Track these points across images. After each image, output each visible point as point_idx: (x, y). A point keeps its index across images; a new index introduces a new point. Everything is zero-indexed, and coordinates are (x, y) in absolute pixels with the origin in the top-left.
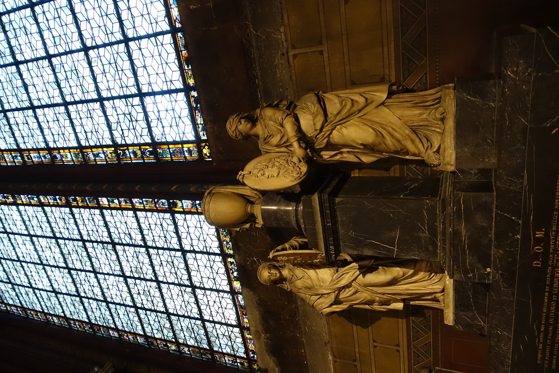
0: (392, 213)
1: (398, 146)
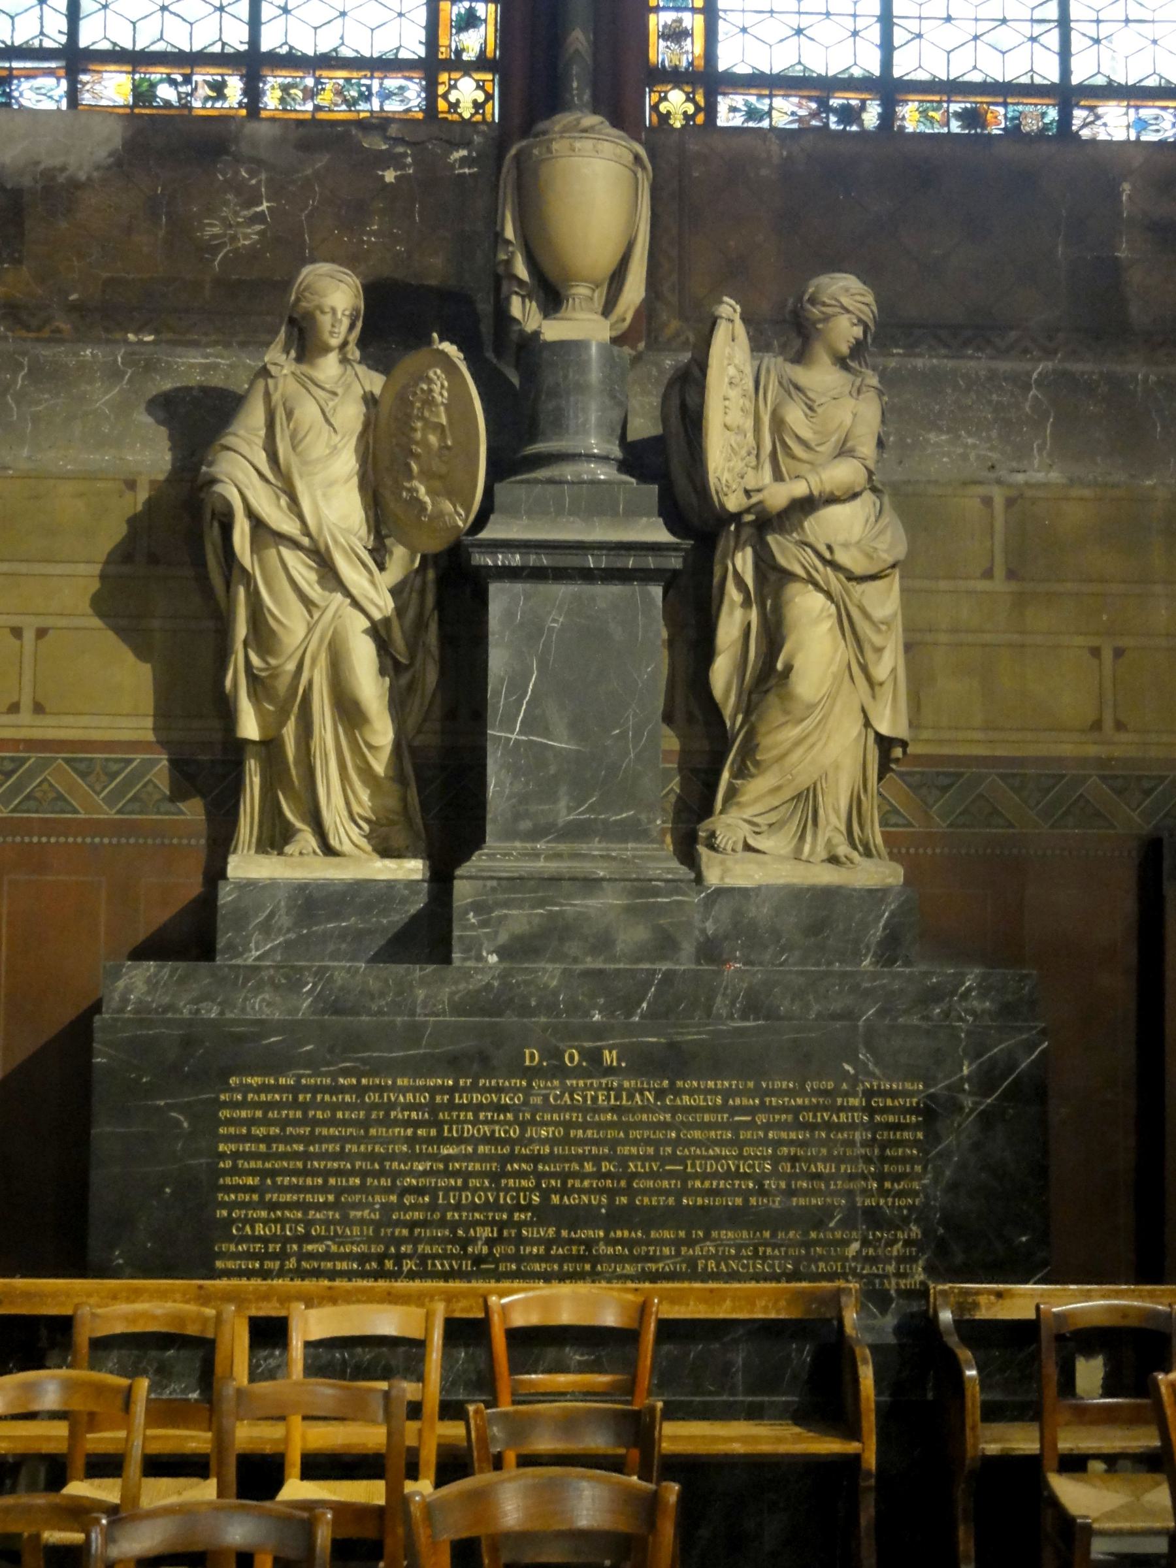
0: (623, 736)
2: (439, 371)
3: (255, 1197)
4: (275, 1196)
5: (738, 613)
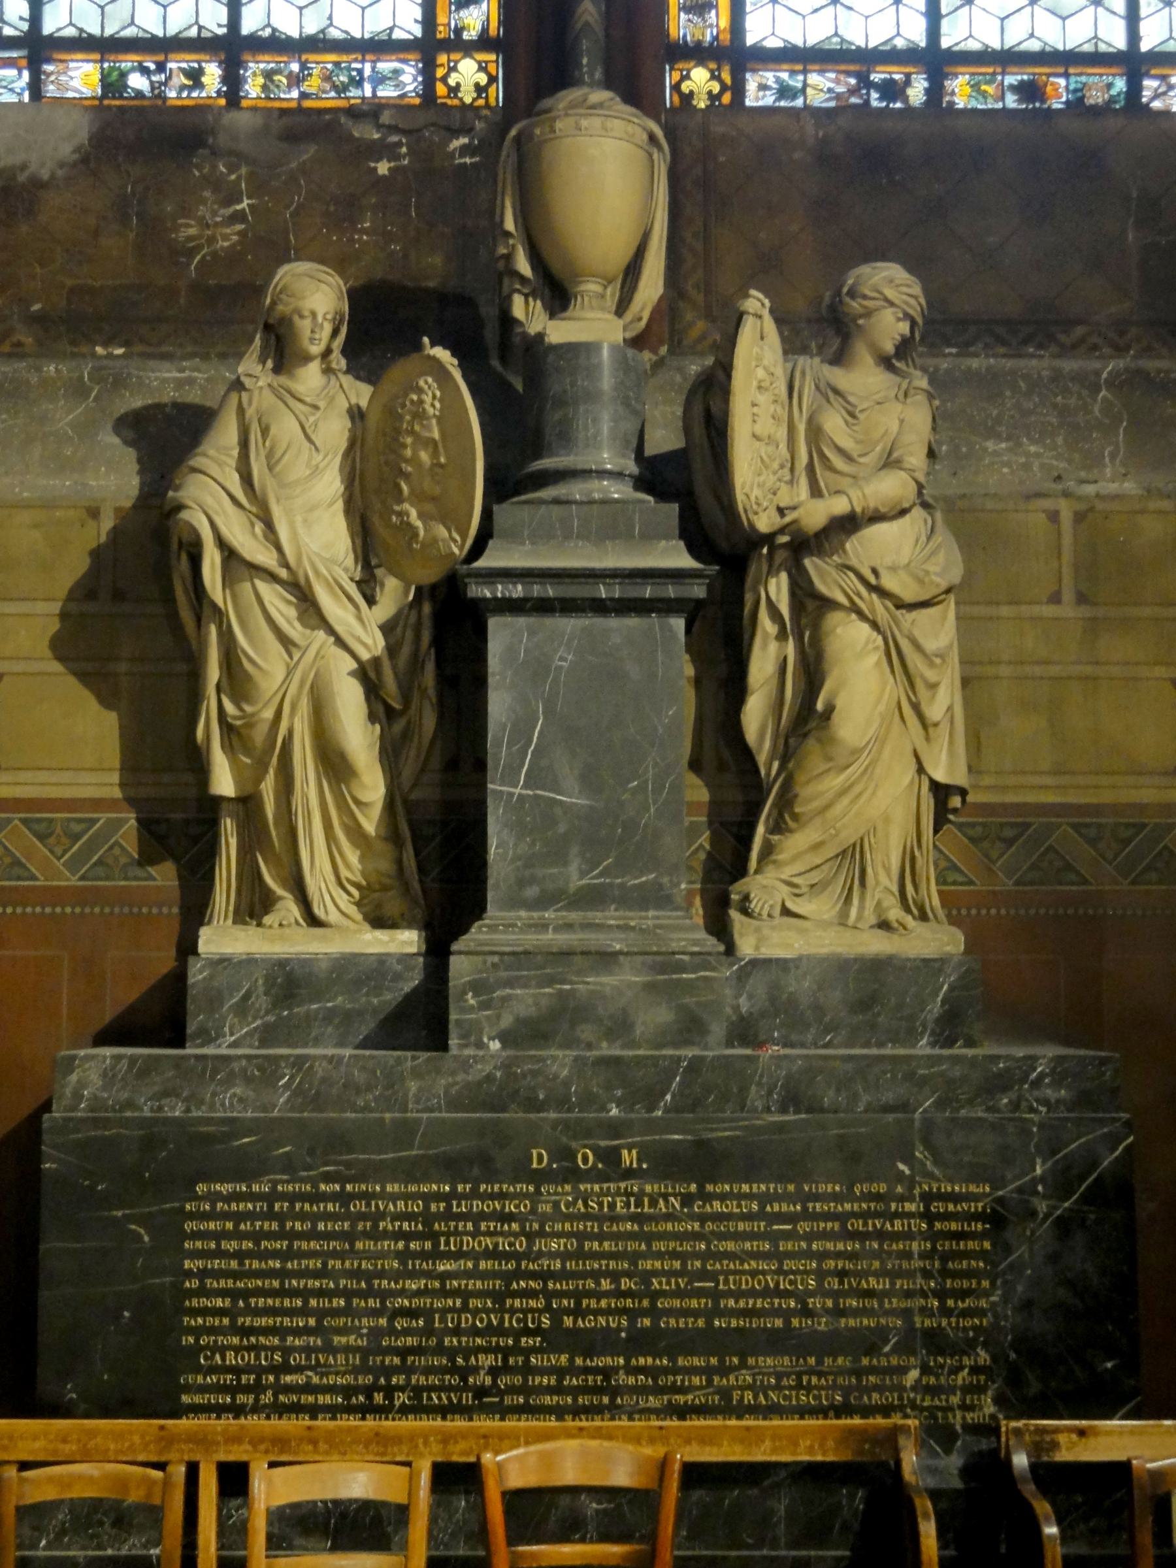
0: (642, 788)
2: (430, 380)
3: (226, 1321)
5: (773, 646)
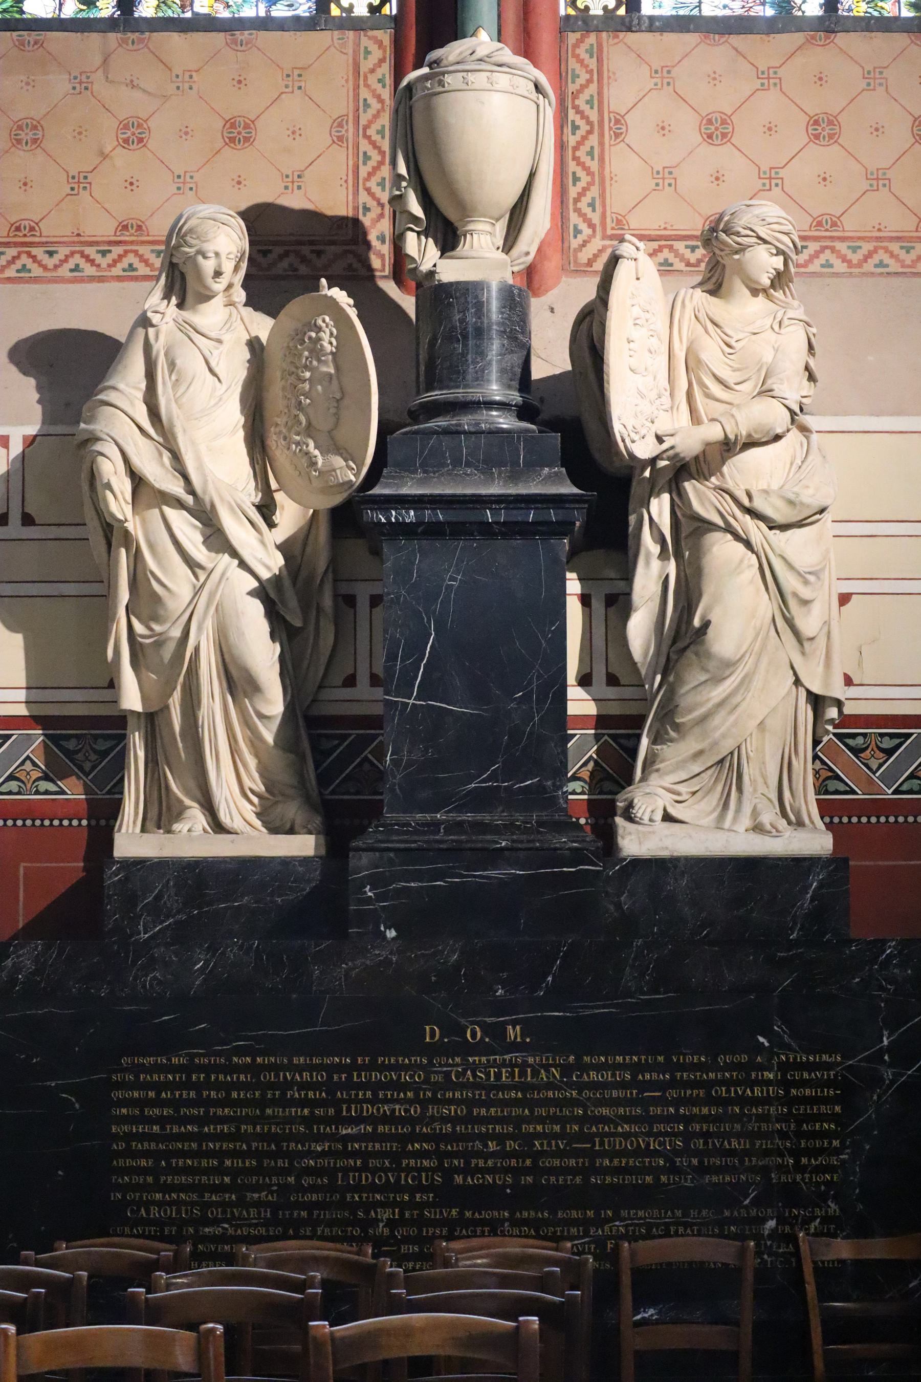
0: (527, 698)
1: (690, 717)
2: (327, 319)
3: (150, 1179)
4: (170, 1178)
5: (656, 564)
